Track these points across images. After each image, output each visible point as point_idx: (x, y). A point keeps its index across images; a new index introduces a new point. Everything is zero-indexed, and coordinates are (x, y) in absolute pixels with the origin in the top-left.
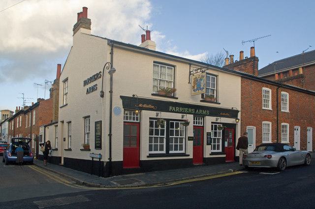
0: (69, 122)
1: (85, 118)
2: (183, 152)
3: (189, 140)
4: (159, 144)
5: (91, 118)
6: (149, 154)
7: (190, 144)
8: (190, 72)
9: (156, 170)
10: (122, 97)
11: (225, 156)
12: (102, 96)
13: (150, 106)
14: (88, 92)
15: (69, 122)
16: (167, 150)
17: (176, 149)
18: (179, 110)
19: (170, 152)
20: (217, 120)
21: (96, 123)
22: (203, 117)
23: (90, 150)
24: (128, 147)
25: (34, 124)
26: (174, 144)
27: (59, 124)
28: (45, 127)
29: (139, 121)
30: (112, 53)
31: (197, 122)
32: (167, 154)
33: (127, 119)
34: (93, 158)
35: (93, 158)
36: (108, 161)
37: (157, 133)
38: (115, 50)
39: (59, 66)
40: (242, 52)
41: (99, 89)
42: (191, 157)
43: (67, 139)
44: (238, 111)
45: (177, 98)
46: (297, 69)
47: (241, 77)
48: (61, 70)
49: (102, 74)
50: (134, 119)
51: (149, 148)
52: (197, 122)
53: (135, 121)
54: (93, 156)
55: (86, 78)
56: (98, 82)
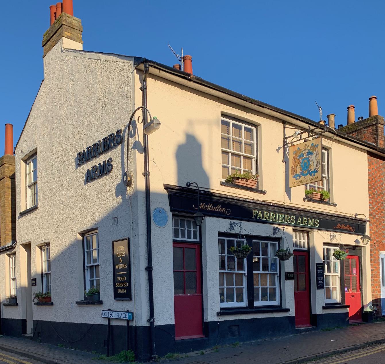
2: (276, 303)
3: (287, 279)
6: (221, 309)
7: (289, 286)
8: (285, 138)
9: (31, 356)
14: (90, 177)
16: (251, 302)
18: (269, 217)
19: (256, 304)
20: (232, 226)
22: (308, 232)
23: (101, 303)
24: (297, 292)
29: (198, 240)
30: (143, 89)
31: (189, 232)
32: (251, 309)
33: (183, 236)
34: (109, 320)
35: (109, 320)
36: (147, 324)
38: (150, 81)
42: (292, 313)
43: (39, 281)
44: (365, 221)
45: (263, 193)
47: (370, 153)
51: (329, 299)
52: (189, 232)
53: (192, 240)
54: (109, 315)
55: (83, 148)
56: (114, 154)
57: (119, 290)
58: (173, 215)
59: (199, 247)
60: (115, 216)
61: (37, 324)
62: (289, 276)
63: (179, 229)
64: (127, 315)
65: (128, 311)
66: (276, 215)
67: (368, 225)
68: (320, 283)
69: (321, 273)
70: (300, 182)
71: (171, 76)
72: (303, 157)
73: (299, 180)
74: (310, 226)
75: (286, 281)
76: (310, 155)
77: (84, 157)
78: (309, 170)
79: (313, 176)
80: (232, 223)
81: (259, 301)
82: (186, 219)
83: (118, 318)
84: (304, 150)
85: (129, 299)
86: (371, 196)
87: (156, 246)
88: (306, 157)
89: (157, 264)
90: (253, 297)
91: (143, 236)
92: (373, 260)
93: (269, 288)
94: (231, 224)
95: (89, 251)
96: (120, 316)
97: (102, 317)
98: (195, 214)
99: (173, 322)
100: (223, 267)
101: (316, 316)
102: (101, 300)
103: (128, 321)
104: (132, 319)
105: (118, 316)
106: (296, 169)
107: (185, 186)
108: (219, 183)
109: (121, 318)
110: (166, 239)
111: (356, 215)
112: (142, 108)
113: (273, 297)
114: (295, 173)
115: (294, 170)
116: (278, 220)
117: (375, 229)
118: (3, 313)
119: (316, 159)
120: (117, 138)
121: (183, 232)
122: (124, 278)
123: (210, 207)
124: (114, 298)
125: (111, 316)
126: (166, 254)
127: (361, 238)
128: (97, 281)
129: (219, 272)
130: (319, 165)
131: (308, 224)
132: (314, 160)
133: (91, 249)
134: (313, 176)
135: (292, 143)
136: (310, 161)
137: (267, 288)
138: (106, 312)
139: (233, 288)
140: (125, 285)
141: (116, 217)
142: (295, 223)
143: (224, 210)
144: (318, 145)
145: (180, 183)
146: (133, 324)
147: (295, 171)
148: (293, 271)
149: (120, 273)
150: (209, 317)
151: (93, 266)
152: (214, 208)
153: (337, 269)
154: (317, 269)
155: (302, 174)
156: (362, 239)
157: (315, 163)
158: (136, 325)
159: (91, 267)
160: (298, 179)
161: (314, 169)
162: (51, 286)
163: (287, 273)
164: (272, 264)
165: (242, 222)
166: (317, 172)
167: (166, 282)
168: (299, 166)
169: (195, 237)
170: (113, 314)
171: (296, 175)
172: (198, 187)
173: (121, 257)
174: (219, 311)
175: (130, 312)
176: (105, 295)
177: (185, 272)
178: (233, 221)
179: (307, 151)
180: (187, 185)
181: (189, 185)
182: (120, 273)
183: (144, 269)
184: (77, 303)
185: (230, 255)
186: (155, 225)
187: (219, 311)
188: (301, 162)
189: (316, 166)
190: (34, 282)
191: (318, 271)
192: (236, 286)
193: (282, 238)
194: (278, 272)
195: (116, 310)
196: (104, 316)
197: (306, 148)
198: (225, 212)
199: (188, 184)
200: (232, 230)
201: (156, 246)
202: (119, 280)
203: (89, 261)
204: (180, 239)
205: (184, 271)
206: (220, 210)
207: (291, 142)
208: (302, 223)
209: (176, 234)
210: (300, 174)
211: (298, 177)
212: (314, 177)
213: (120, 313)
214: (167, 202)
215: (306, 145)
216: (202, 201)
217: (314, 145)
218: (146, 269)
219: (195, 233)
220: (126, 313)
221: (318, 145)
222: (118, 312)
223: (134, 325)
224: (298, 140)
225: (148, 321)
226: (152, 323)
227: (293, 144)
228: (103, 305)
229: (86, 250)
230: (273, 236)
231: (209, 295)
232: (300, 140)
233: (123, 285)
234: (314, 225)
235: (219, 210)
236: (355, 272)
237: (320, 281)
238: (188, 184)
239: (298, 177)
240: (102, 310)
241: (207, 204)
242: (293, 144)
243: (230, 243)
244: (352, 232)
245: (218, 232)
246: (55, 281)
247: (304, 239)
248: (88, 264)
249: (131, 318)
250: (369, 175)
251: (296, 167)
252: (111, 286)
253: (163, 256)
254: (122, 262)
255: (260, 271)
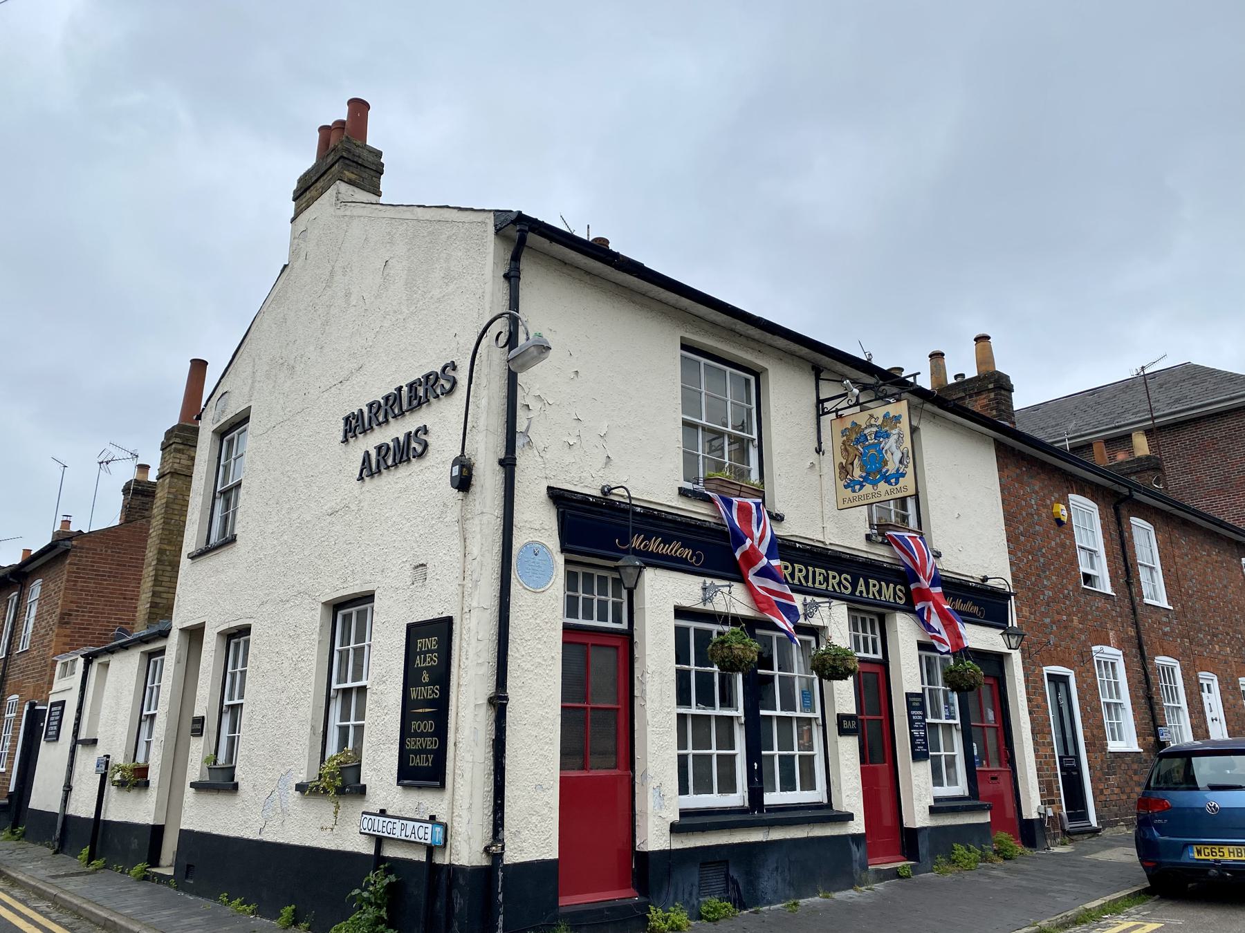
0: (237, 636)
1: (337, 607)
2: (816, 796)
3: (843, 732)
4: (796, 752)
5: (252, 637)
7: (848, 750)
10: (557, 496)
11: (986, 818)
12: (463, 483)
13: (675, 549)
14: (370, 469)
15: (237, 636)
16: (756, 794)
17: (788, 785)
19: (770, 798)
21: (415, 631)
25: (24, 645)
26: (776, 752)
27: (173, 644)
28: (89, 660)
29: (624, 626)
33: (588, 615)
34: (379, 841)
36: (481, 861)
37: (705, 699)
39: (199, 366)
40: (937, 356)
41: (444, 448)
42: (858, 826)
43: (210, 725)
44: (1007, 596)
46: (1127, 437)
48: (203, 402)
49: (462, 376)
50: (602, 617)
53: (610, 624)
54: (381, 826)
55: (359, 404)
57: (413, 757)
58: (567, 562)
59: (625, 644)
60: (421, 563)
61: (189, 838)
62: (846, 725)
63: (578, 598)
64: (429, 831)
65: (432, 818)
66: (808, 571)
67: (1012, 604)
68: (919, 745)
69: (920, 718)
70: (862, 499)
71: (574, 256)
72: (867, 443)
73: (858, 494)
74: (886, 601)
75: (839, 738)
76: (881, 439)
77: (358, 425)
78: (884, 470)
79: (893, 484)
80: (707, 585)
81: (774, 790)
82: (597, 573)
83: (403, 837)
84: (866, 428)
85: (438, 783)
86: (1012, 539)
87: (519, 638)
88: (873, 444)
89: (521, 688)
90: (761, 781)
91: (489, 611)
92: (1030, 688)
93: (800, 756)
94: (704, 589)
95: (344, 650)
96: (409, 833)
97: (361, 833)
98: (619, 562)
99: (554, 854)
100: (683, 699)
101: (914, 833)
102: (362, 782)
103: (430, 850)
104: (442, 843)
105: (403, 832)
106: (851, 469)
107: (598, 493)
108: (677, 491)
109: (412, 839)
110: (546, 620)
111: (985, 579)
112: (506, 315)
113: (809, 784)
114: (848, 477)
115: (846, 470)
116: (814, 582)
117: (1028, 614)
118: (106, 807)
119: (898, 448)
120: (442, 382)
121: (588, 603)
122: (429, 726)
123: (654, 546)
124: (399, 779)
125: (385, 830)
126: (545, 660)
127: (1001, 634)
128: (359, 729)
129: (678, 714)
130: (908, 461)
131: (880, 596)
132: (894, 449)
133: (367, 642)
134: (893, 484)
135: (837, 411)
136: (884, 452)
137: (793, 756)
138: (373, 817)
139: (710, 756)
140: (432, 743)
141: (422, 565)
142: (853, 593)
143: (688, 553)
144: (900, 416)
145: (587, 486)
146: (441, 859)
147: (848, 474)
148: (854, 712)
149: (421, 711)
150: (651, 837)
151: (351, 689)
152: (666, 547)
153: (952, 708)
154: (910, 707)
155: (865, 479)
156: (1006, 636)
157: (898, 455)
158: (453, 862)
159: (346, 692)
160: (857, 491)
161: (895, 469)
162: (239, 736)
163: (841, 718)
164: (803, 692)
165: (732, 583)
166: (903, 475)
167: (541, 737)
168: (856, 461)
169: (617, 619)
170: (390, 826)
171: (850, 480)
172: (630, 497)
173: (426, 668)
174: (676, 818)
175: (440, 824)
176: (375, 769)
177: (589, 710)
178: (709, 581)
179: (874, 429)
180: (602, 491)
181: (607, 491)
182: (421, 711)
183: (486, 701)
184: (300, 788)
185: (703, 668)
186: (521, 585)
187: (676, 818)
188: (861, 454)
189: (901, 462)
190: (198, 726)
191: (913, 712)
192: (717, 749)
193: (824, 627)
194: (818, 714)
195: (398, 814)
196: (367, 831)
197: (873, 422)
198: (691, 559)
199: (606, 490)
200: (708, 604)
201: (519, 638)
202: (415, 730)
203: (343, 675)
204: (580, 621)
205: (585, 708)
206: (680, 554)
207: (834, 409)
208: (868, 593)
209: (571, 609)
210: (861, 480)
211: (857, 487)
212: (898, 486)
213: (411, 824)
214: (553, 529)
215: (872, 416)
216: (638, 531)
217: (891, 416)
218: (491, 701)
219: (617, 608)
220: (425, 825)
221: (900, 416)
222: (405, 822)
223: (447, 862)
224: (850, 406)
225: (487, 850)
226: (497, 858)
227: (840, 413)
228: (367, 796)
229: (337, 647)
230: (805, 622)
231: (650, 772)
232: (855, 405)
233: (426, 746)
234: (895, 599)
235: (678, 553)
236: (991, 715)
237: (918, 738)
238: (606, 490)
239: (857, 487)
240: (364, 813)
241: (648, 538)
242: (840, 413)
243: (703, 636)
244: (979, 618)
245: (675, 606)
246: (250, 725)
247: (873, 632)
248: (339, 682)
249: (439, 837)
250: (1002, 491)
251: (850, 464)
252: (392, 744)
253: (536, 667)
254: (427, 680)
255: (776, 710)
